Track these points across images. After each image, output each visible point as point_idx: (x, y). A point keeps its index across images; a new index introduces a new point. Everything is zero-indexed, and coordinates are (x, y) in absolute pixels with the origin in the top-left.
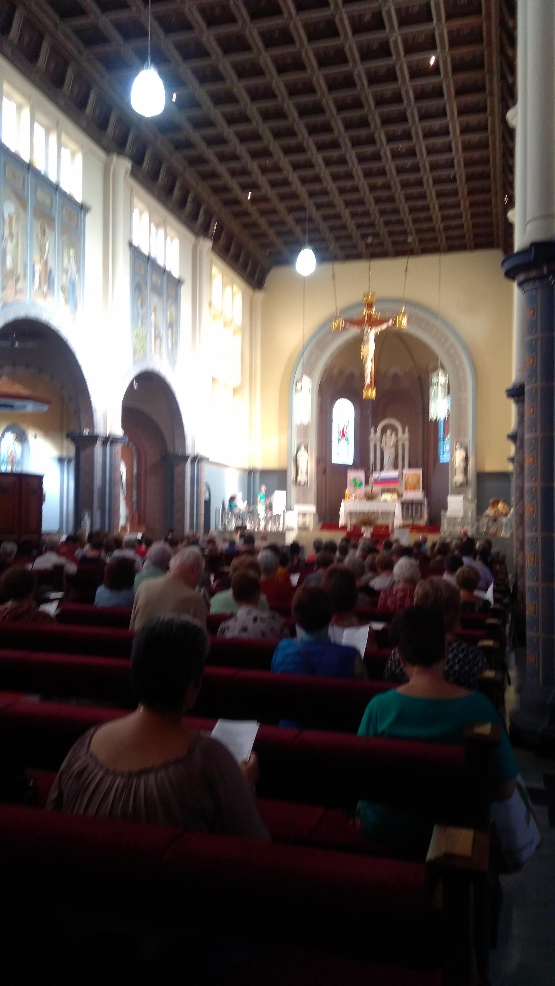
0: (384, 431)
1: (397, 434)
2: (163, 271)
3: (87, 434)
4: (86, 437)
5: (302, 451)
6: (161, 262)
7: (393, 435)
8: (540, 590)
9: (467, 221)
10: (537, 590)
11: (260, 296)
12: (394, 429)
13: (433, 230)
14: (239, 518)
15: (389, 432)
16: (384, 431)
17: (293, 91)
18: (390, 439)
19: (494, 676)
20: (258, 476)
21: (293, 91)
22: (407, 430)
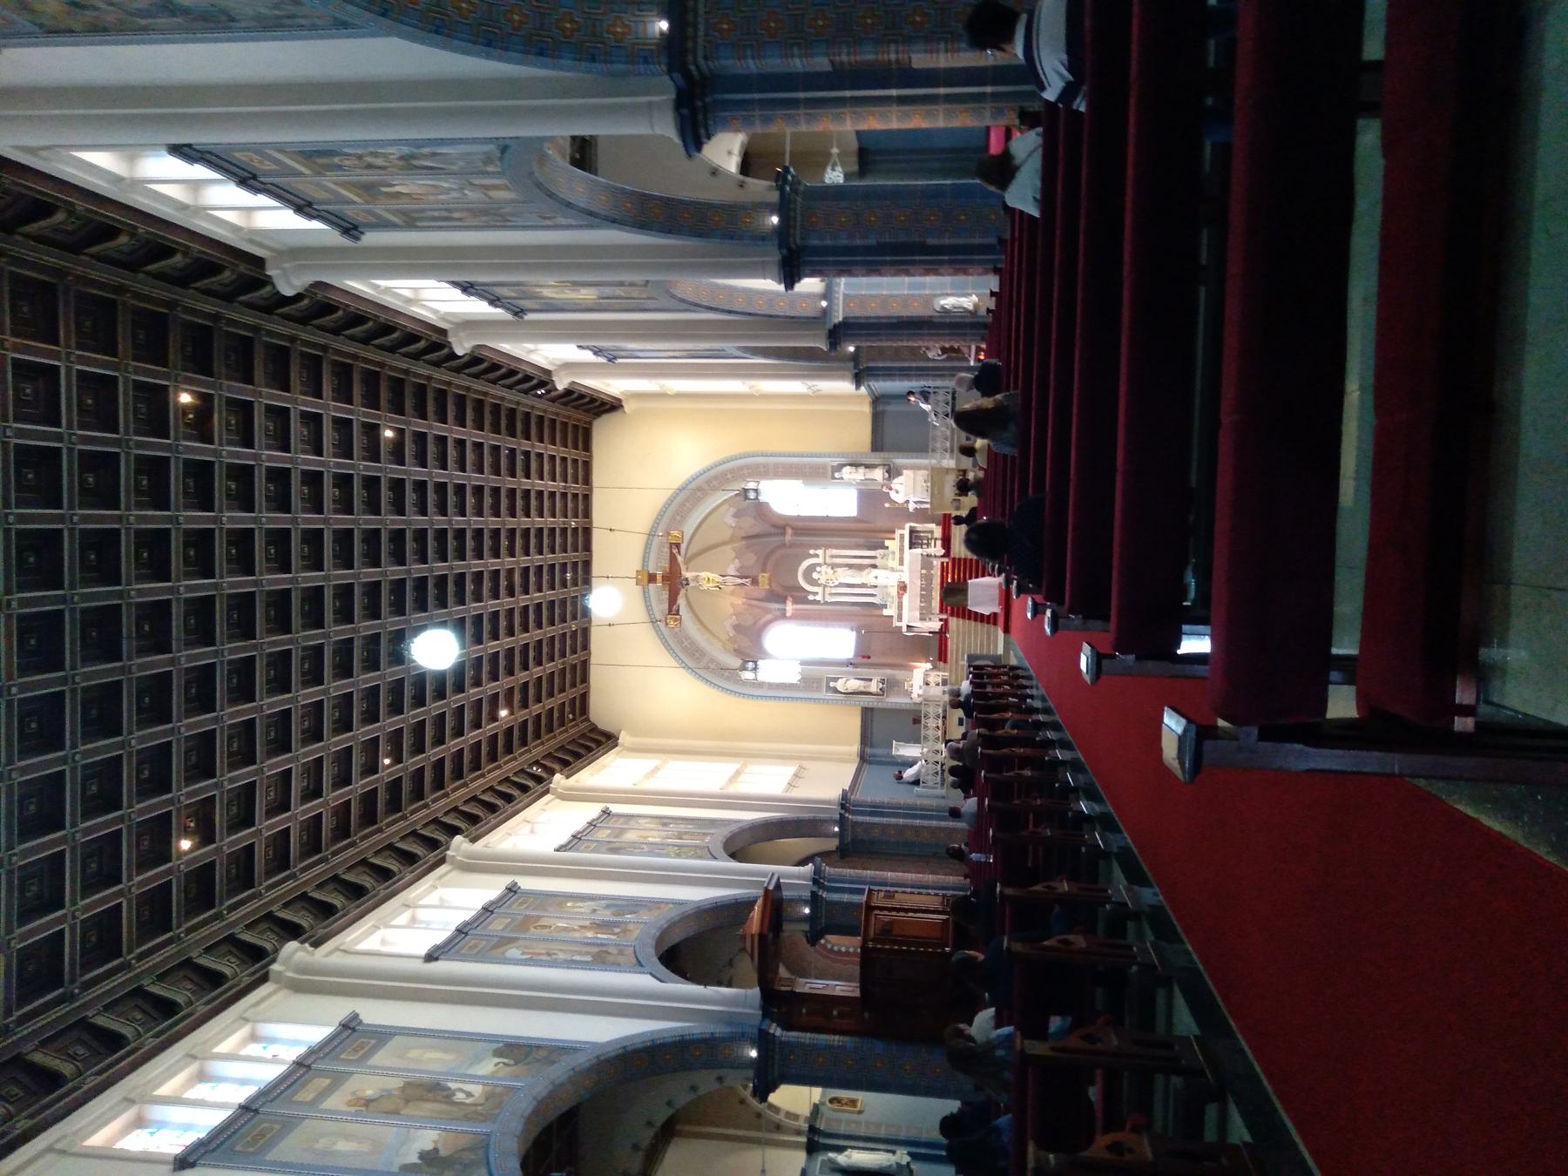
0: (814, 583)
1: (820, 565)
2: (488, 910)
3: (858, 985)
4: (863, 989)
5: (840, 685)
6: (467, 916)
7: (818, 569)
8: (993, 105)
9: (557, 451)
10: (995, 108)
11: (624, 738)
12: (812, 568)
13: (564, 495)
14: (336, 160)
15: (815, 576)
16: (814, 583)
17: (344, 670)
18: (822, 575)
19: (976, 808)
20: (868, 750)
21: (344, 670)
22: (812, 552)
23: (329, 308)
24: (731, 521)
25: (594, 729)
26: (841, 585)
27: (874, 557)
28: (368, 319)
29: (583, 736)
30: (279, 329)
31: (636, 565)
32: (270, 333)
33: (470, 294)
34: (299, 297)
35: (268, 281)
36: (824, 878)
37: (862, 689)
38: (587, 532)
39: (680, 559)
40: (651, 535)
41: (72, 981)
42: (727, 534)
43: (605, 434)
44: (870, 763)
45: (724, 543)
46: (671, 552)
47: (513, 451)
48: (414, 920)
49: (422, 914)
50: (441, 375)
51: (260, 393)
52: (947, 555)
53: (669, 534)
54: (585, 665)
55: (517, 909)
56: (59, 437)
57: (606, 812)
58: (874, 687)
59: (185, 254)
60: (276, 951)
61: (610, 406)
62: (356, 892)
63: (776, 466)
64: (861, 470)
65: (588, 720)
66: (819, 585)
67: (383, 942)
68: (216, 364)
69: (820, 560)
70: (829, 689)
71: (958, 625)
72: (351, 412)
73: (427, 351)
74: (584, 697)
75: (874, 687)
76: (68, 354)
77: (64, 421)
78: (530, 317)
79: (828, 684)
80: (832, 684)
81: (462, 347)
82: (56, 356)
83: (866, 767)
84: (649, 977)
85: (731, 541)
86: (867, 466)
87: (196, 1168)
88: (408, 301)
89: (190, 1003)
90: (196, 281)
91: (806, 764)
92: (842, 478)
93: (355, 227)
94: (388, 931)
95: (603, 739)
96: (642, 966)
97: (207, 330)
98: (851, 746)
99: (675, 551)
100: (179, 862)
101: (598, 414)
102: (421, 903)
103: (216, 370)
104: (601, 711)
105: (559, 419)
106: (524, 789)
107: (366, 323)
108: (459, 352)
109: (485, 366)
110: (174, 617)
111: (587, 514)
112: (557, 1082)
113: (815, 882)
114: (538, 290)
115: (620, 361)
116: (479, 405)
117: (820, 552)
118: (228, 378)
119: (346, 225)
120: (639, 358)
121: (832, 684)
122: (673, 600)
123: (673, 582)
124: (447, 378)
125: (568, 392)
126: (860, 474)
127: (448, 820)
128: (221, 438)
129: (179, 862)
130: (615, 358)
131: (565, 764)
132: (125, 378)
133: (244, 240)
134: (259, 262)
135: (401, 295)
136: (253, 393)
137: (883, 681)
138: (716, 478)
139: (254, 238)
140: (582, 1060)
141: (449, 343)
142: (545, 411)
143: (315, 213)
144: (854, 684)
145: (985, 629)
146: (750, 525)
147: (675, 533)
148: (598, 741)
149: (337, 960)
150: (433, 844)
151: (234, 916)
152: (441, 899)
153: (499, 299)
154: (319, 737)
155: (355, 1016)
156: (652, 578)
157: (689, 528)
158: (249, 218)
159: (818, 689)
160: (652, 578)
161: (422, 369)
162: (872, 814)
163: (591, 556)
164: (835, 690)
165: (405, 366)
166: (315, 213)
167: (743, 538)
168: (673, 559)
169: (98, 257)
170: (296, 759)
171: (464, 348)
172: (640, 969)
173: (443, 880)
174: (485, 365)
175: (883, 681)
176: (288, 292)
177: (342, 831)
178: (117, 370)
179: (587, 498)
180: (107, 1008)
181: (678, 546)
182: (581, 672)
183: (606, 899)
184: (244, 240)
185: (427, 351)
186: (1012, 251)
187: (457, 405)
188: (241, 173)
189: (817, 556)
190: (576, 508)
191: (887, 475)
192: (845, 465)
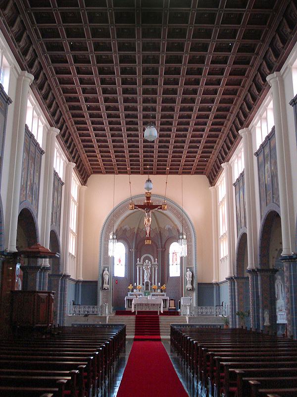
12: (150, 260)
16: (144, 261)
23: (259, 90)
24: (167, 227)
25: (88, 176)
26: (143, 271)
27: (155, 284)
29: (86, 172)
30: (252, 73)
32: (250, 70)
36: (45, 271)
37: (105, 281)
38: (164, 173)
39: (156, 209)
40: (165, 198)
42: (162, 226)
43: (203, 179)
44: (76, 284)
45: (158, 224)
46: (159, 206)
47: (198, 147)
50: (229, 124)
51: (230, 67)
52: (161, 314)
53: (165, 205)
54: (113, 173)
55: (38, 153)
56: (222, 7)
57: (63, 184)
58: (105, 286)
60: (31, 73)
61: (212, 180)
62: (45, 97)
63: (191, 245)
64: (191, 279)
65: (92, 174)
66: (143, 263)
68: (240, 53)
69: (153, 263)
70: (105, 267)
71: (132, 319)
72: (220, 94)
73: (240, 120)
74: (101, 173)
75: (105, 286)
76: (250, 11)
77: (227, 9)
79: (106, 267)
80: (106, 269)
82: (249, 8)
83: (73, 283)
85: (159, 228)
86: (192, 281)
88: (261, 116)
91: (76, 259)
92: (187, 271)
94: (32, 109)
95: (84, 180)
97: (253, 51)
98: (213, 287)
99: (159, 207)
100: (36, 26)
101: (208, 177)
103: (239, 53)
104: (94, 179)
105: (208, 164)
106: (71, 153)
107: (253, 101)
110: (155, 39)
111: (171, 173)
113: (44, 268)
114: (269, 163)
117: (156, 263)
118: (236, 57)
121: (106, 269)
122: (140, 206)
123: (148, 207)
124: (228, 126)
126: (189, 279)
127: (64, 127)
128: (215, 54)
129: (36, 26)
130: (235, 186)
131: (77, 167)
132: (217, 11)
133: (288, 66)
134: (279, 70)
136: (230, 64)
137: (108, 289)
138: (186, 222)
139: (288, 69)
141: (243, 128)
142: (211, 159)
144: (106, 278)
145: (133, 330)
146: (166, 235)
147: (166, 207)
148: (84, 180)
150: (57, 122)
151: (43, 58)
153: (263, 148)
154: (79, 73)
156: (148, 198)
157: (167, 212)
159: (104, 264)
160: (148, 198)
161: (232, 117)
162: (61, 287)
163: (155, 174)
164: (103, 271)
165: (234, 112)
167: (160, 232)
168: (156, 206)
170: (71, 65)
173: (14, 68)
174: (233, 139)
175: (108, 289)
176: (268, 78)
177: (65, 91)
178: (243, 24)
179: (177, 173)
181: (161, 208)
182: (110, 171)
183: (39, 187)
184: (288, 66)
185: (240, 120)
186: (100, 342)
189: (155, 261)
190: (174, 169)
191: (189, 289)
192: (192, 273)
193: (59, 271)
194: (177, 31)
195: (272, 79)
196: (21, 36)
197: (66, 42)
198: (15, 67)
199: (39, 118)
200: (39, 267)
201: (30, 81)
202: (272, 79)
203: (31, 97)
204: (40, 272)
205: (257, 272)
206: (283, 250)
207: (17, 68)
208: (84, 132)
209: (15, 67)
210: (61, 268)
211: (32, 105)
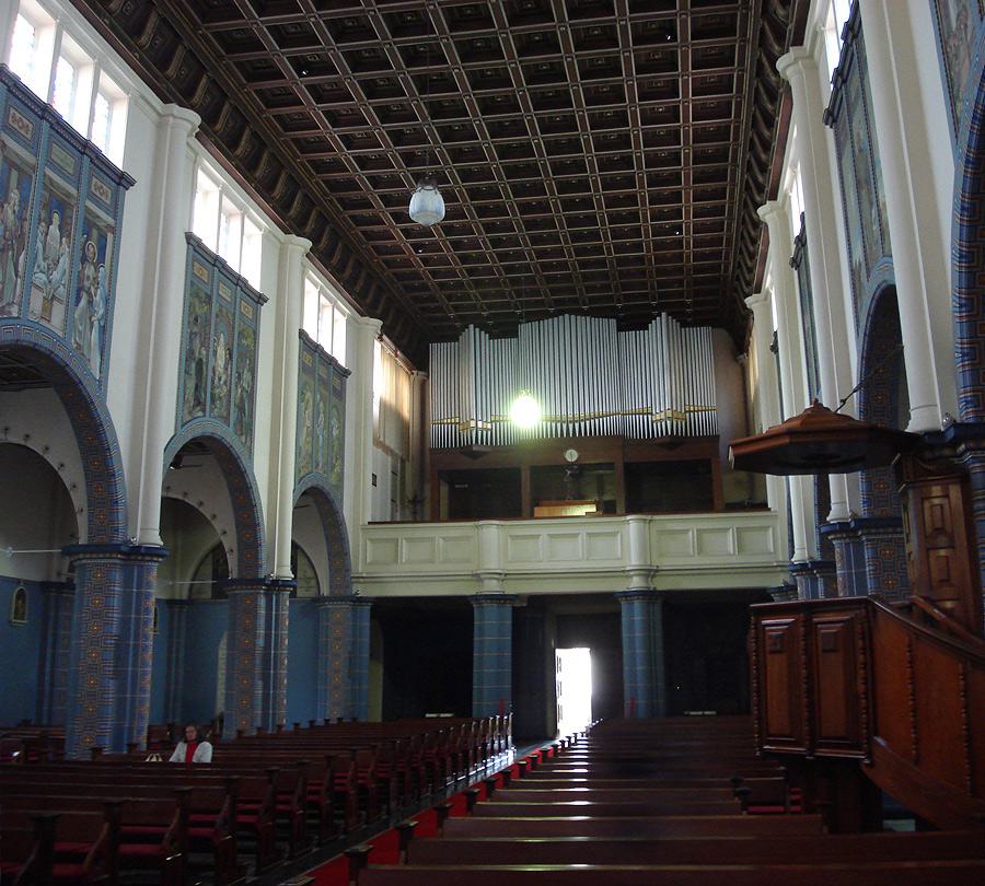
6: (233, 264)
23: (773, 98)
28: (771, 131)
31: (666, 563)
33: (845, 37)
34: (776, 73)
35: (784, 51)
41: (207, 28)
48: (229, 216)
49: (236, 223)
59: (787, 17)
67: (206, 193)
78: (830, 132)
81: (765, 212)
84: (173, 434)
87: (186, 245)
89: (168, 78)
90: (765, 54)
93: (834, 121)
96: (183, 426)
102: (246, 219)
104: (439, 352)
108: (761, 211)
109: (771, 97)
112: (67, 369)
115: (796, 272)
116: (721, 155)
119: (845, 72)
120: (840, 158)
125: (758, 224)
130: (798, 267)
135: (826, 14)
140: (244, 461)
143: (849, 42)
148: (415, 357)
149: (182, 152)
152: (324, 306)
155: (132, 183)
158: (831, 29)
166: (849, 42)
169: (763, 32)
171: (764, 215)
172: (298, 479)
173: (141, 101)
180: (164, 20)
187: (712, 253)
188: (845, 72)
193: (257, 566)
194: (537, 38)
195: (789, 65)
196: (257, 159)
197: (300, 84)
198: (143, 97)
199: (335, 306)
200: (262, 581)
201: (190, 126)
202: (789, 65)
203: (313, 274)
204: (266, 595)
205: (855, 531)
206: (833, 507)
207: (147, 96)
208: (376, 228)
209: (143, 97)
210: (263, 555)
211: (316, 285)
